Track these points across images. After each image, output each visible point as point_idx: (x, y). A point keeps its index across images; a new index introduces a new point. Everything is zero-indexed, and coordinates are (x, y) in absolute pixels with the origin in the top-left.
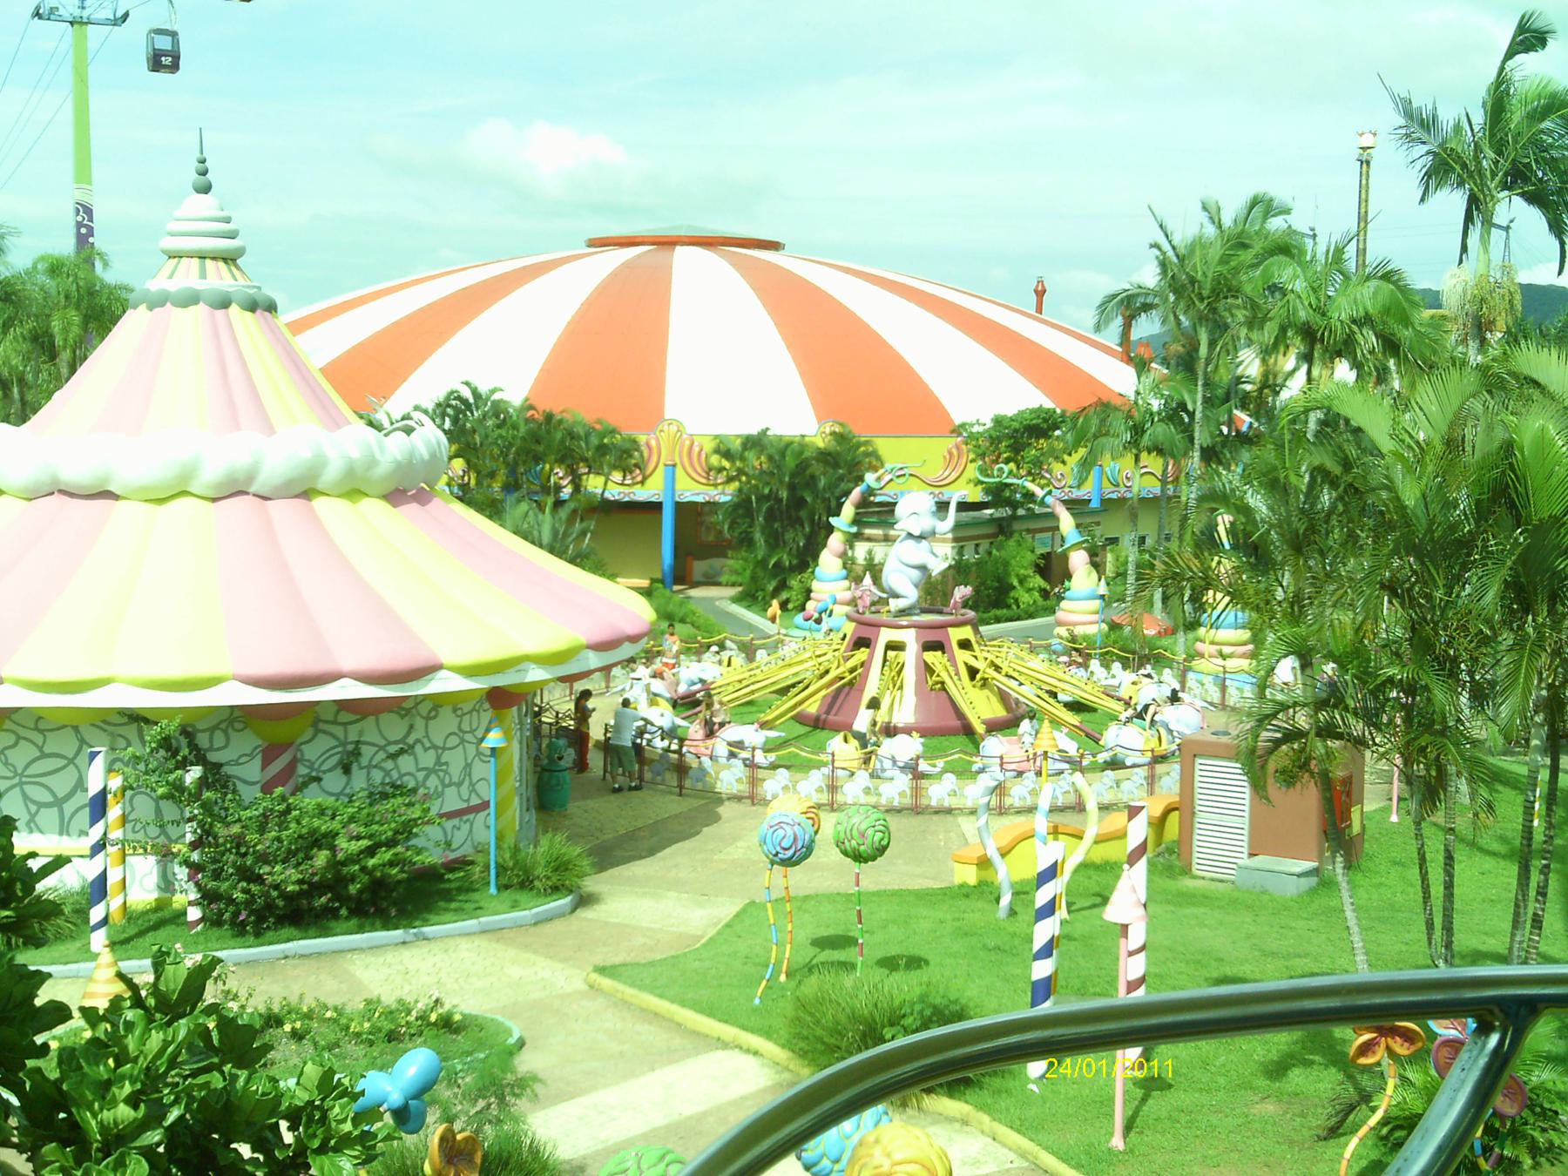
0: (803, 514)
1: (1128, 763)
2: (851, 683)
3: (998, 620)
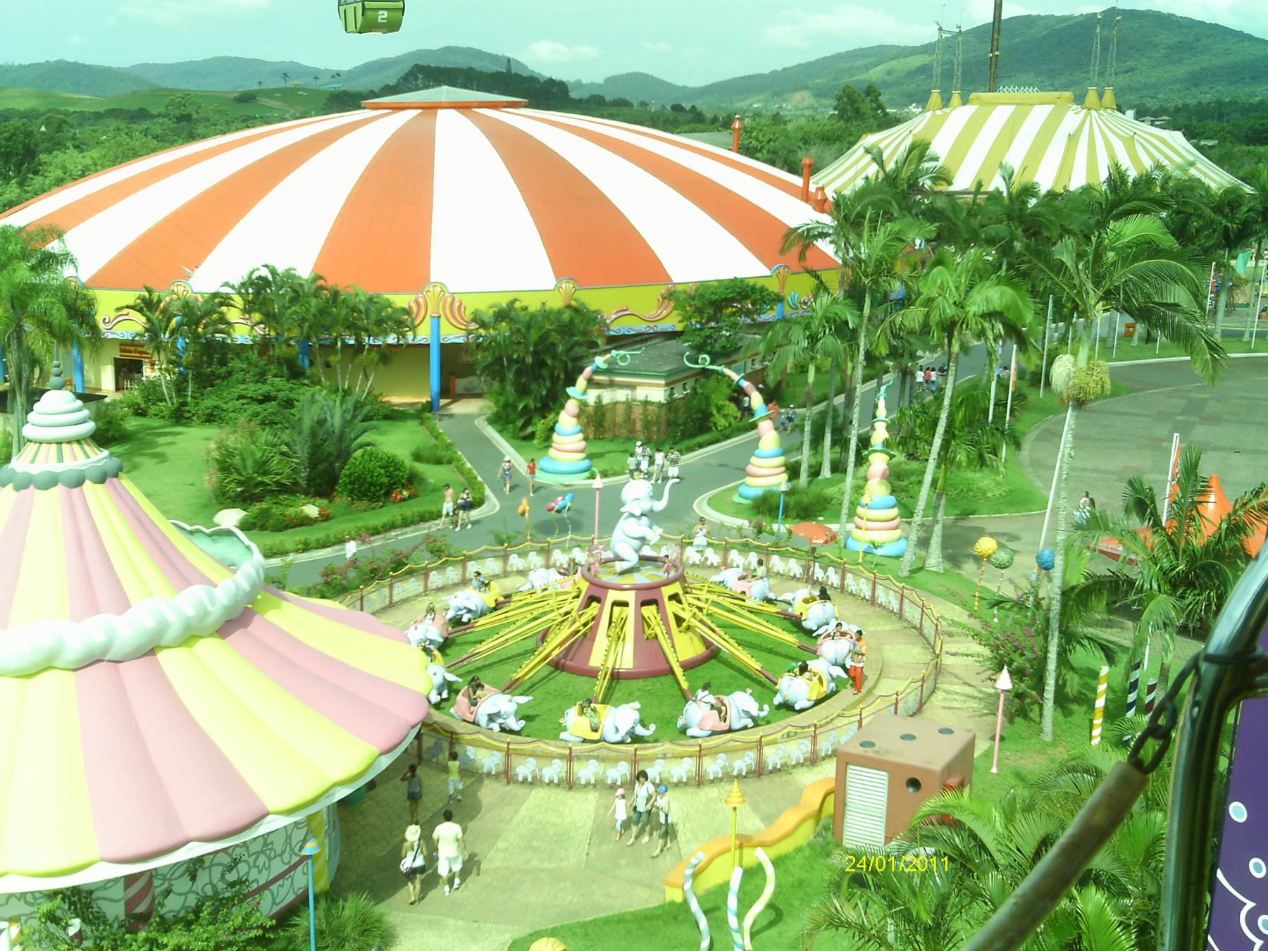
0: (545, 373)
1: (797, 707)
2: (585, 635)
3: (701, 446)
